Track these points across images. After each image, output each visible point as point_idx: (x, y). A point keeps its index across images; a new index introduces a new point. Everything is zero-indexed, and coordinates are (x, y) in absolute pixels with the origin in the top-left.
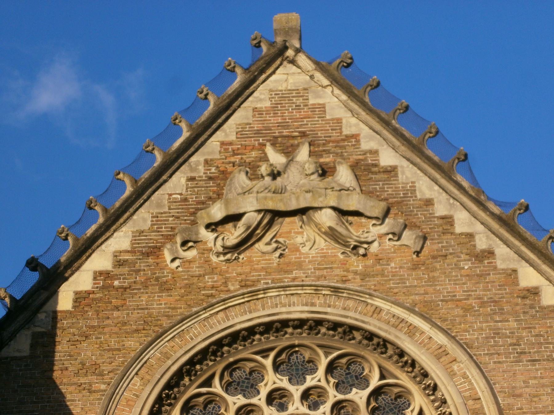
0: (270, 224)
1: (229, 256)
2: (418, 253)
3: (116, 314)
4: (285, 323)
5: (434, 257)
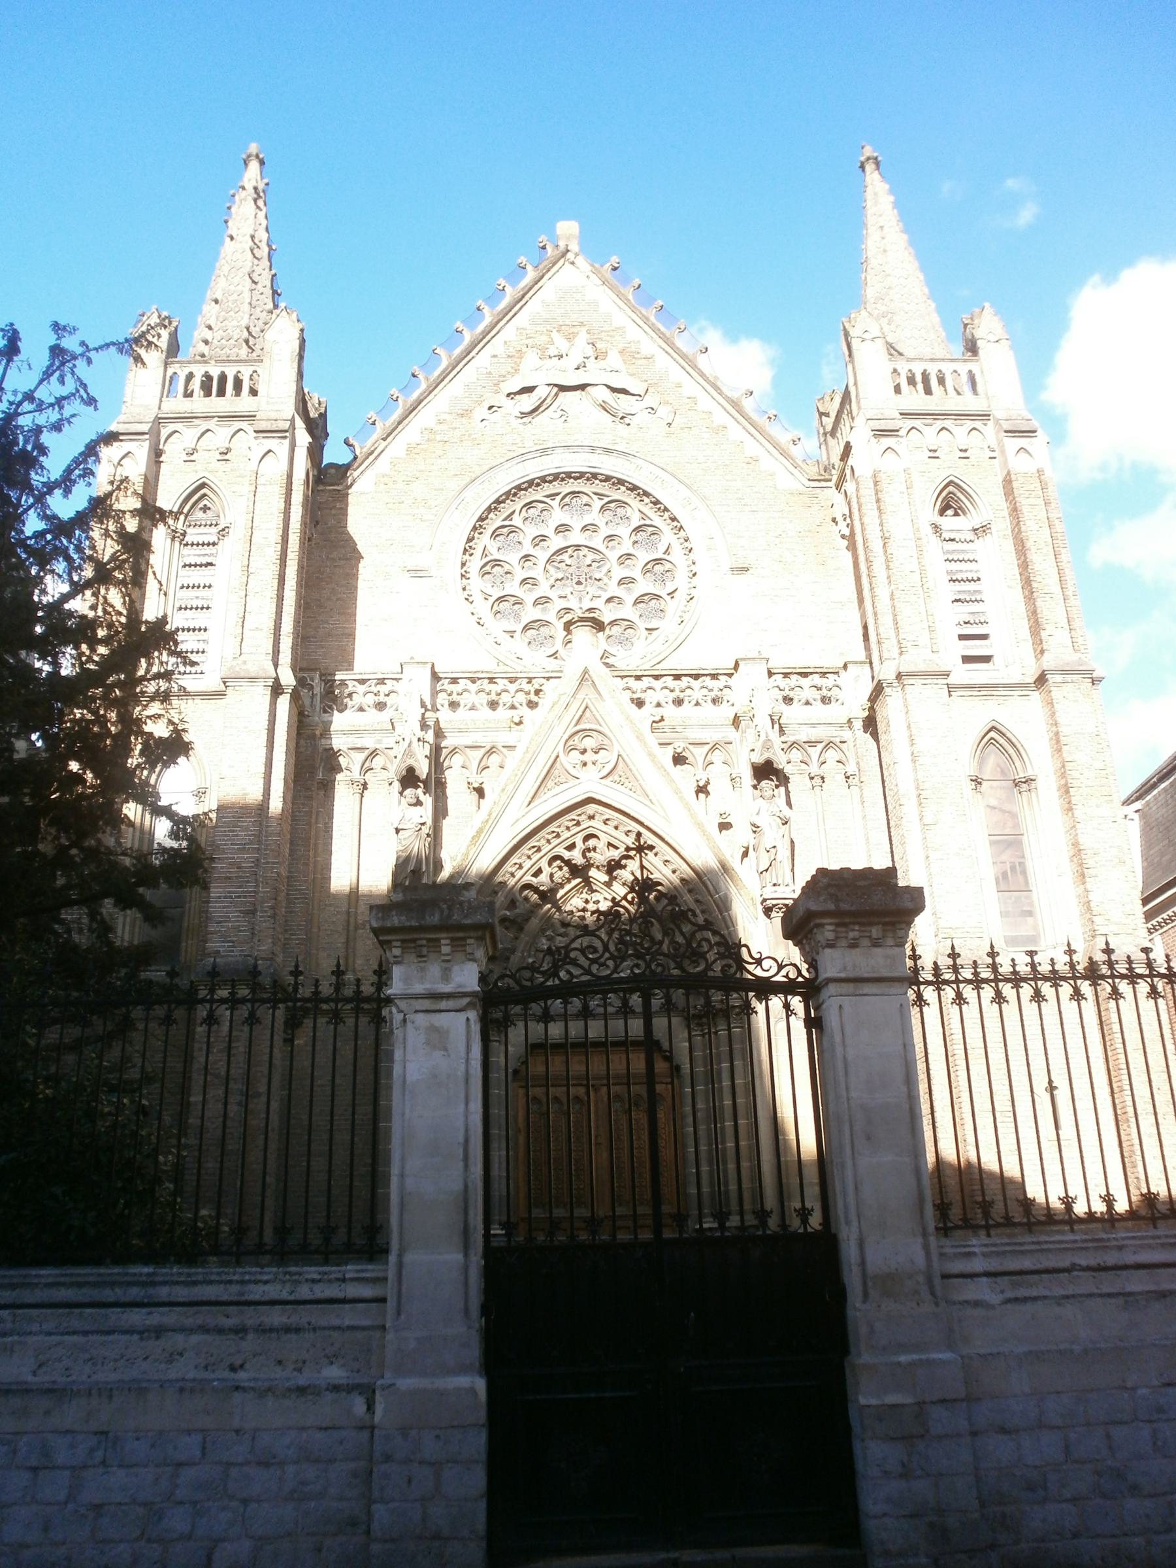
1: (525, 420)
2: (670, 424)
4: (569, 475)
5: (682, 429)
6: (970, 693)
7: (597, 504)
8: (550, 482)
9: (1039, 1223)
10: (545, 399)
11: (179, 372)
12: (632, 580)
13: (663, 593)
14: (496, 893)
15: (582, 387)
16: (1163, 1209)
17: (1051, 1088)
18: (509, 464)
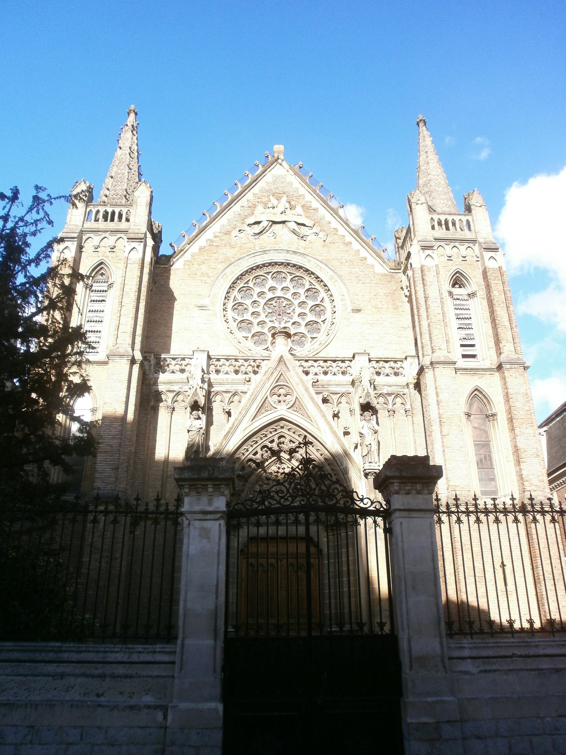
0: (271, 226)
1: (256, 237)
3: (214, 255)
4: (276, 263)
5: (330, 243)
6: (466, 372)
7: (289, 278)
8: (267, 266)
9: (497, 633)
10: (266, 228)
11: (93, 209)
12: (305, 314)
13: (319, 321)
14: (235, 463)
15: (284, 222)
16: (558, 627)
17: (503, 565)
18: (248, 258)
